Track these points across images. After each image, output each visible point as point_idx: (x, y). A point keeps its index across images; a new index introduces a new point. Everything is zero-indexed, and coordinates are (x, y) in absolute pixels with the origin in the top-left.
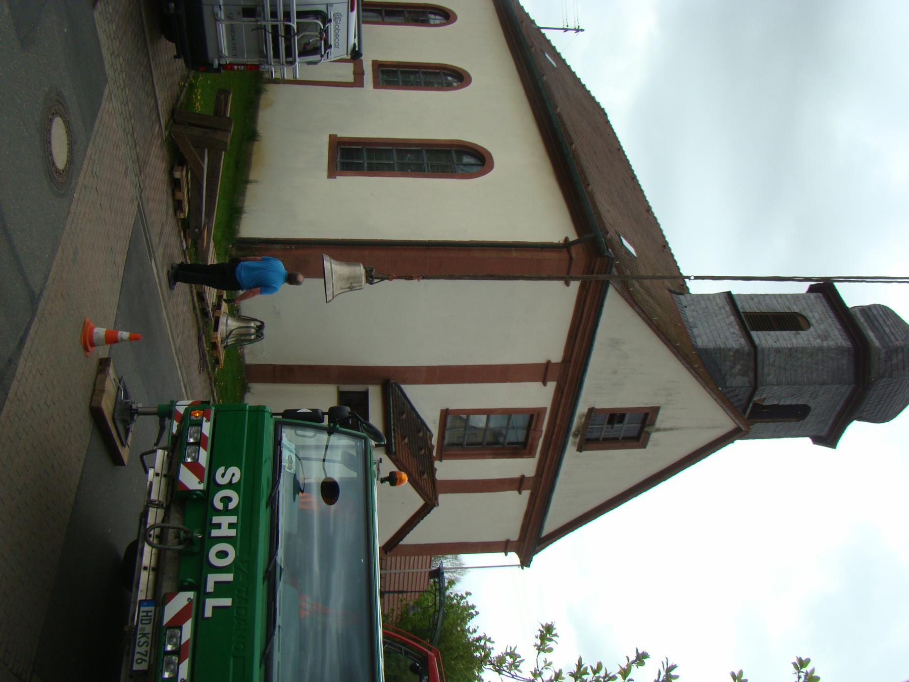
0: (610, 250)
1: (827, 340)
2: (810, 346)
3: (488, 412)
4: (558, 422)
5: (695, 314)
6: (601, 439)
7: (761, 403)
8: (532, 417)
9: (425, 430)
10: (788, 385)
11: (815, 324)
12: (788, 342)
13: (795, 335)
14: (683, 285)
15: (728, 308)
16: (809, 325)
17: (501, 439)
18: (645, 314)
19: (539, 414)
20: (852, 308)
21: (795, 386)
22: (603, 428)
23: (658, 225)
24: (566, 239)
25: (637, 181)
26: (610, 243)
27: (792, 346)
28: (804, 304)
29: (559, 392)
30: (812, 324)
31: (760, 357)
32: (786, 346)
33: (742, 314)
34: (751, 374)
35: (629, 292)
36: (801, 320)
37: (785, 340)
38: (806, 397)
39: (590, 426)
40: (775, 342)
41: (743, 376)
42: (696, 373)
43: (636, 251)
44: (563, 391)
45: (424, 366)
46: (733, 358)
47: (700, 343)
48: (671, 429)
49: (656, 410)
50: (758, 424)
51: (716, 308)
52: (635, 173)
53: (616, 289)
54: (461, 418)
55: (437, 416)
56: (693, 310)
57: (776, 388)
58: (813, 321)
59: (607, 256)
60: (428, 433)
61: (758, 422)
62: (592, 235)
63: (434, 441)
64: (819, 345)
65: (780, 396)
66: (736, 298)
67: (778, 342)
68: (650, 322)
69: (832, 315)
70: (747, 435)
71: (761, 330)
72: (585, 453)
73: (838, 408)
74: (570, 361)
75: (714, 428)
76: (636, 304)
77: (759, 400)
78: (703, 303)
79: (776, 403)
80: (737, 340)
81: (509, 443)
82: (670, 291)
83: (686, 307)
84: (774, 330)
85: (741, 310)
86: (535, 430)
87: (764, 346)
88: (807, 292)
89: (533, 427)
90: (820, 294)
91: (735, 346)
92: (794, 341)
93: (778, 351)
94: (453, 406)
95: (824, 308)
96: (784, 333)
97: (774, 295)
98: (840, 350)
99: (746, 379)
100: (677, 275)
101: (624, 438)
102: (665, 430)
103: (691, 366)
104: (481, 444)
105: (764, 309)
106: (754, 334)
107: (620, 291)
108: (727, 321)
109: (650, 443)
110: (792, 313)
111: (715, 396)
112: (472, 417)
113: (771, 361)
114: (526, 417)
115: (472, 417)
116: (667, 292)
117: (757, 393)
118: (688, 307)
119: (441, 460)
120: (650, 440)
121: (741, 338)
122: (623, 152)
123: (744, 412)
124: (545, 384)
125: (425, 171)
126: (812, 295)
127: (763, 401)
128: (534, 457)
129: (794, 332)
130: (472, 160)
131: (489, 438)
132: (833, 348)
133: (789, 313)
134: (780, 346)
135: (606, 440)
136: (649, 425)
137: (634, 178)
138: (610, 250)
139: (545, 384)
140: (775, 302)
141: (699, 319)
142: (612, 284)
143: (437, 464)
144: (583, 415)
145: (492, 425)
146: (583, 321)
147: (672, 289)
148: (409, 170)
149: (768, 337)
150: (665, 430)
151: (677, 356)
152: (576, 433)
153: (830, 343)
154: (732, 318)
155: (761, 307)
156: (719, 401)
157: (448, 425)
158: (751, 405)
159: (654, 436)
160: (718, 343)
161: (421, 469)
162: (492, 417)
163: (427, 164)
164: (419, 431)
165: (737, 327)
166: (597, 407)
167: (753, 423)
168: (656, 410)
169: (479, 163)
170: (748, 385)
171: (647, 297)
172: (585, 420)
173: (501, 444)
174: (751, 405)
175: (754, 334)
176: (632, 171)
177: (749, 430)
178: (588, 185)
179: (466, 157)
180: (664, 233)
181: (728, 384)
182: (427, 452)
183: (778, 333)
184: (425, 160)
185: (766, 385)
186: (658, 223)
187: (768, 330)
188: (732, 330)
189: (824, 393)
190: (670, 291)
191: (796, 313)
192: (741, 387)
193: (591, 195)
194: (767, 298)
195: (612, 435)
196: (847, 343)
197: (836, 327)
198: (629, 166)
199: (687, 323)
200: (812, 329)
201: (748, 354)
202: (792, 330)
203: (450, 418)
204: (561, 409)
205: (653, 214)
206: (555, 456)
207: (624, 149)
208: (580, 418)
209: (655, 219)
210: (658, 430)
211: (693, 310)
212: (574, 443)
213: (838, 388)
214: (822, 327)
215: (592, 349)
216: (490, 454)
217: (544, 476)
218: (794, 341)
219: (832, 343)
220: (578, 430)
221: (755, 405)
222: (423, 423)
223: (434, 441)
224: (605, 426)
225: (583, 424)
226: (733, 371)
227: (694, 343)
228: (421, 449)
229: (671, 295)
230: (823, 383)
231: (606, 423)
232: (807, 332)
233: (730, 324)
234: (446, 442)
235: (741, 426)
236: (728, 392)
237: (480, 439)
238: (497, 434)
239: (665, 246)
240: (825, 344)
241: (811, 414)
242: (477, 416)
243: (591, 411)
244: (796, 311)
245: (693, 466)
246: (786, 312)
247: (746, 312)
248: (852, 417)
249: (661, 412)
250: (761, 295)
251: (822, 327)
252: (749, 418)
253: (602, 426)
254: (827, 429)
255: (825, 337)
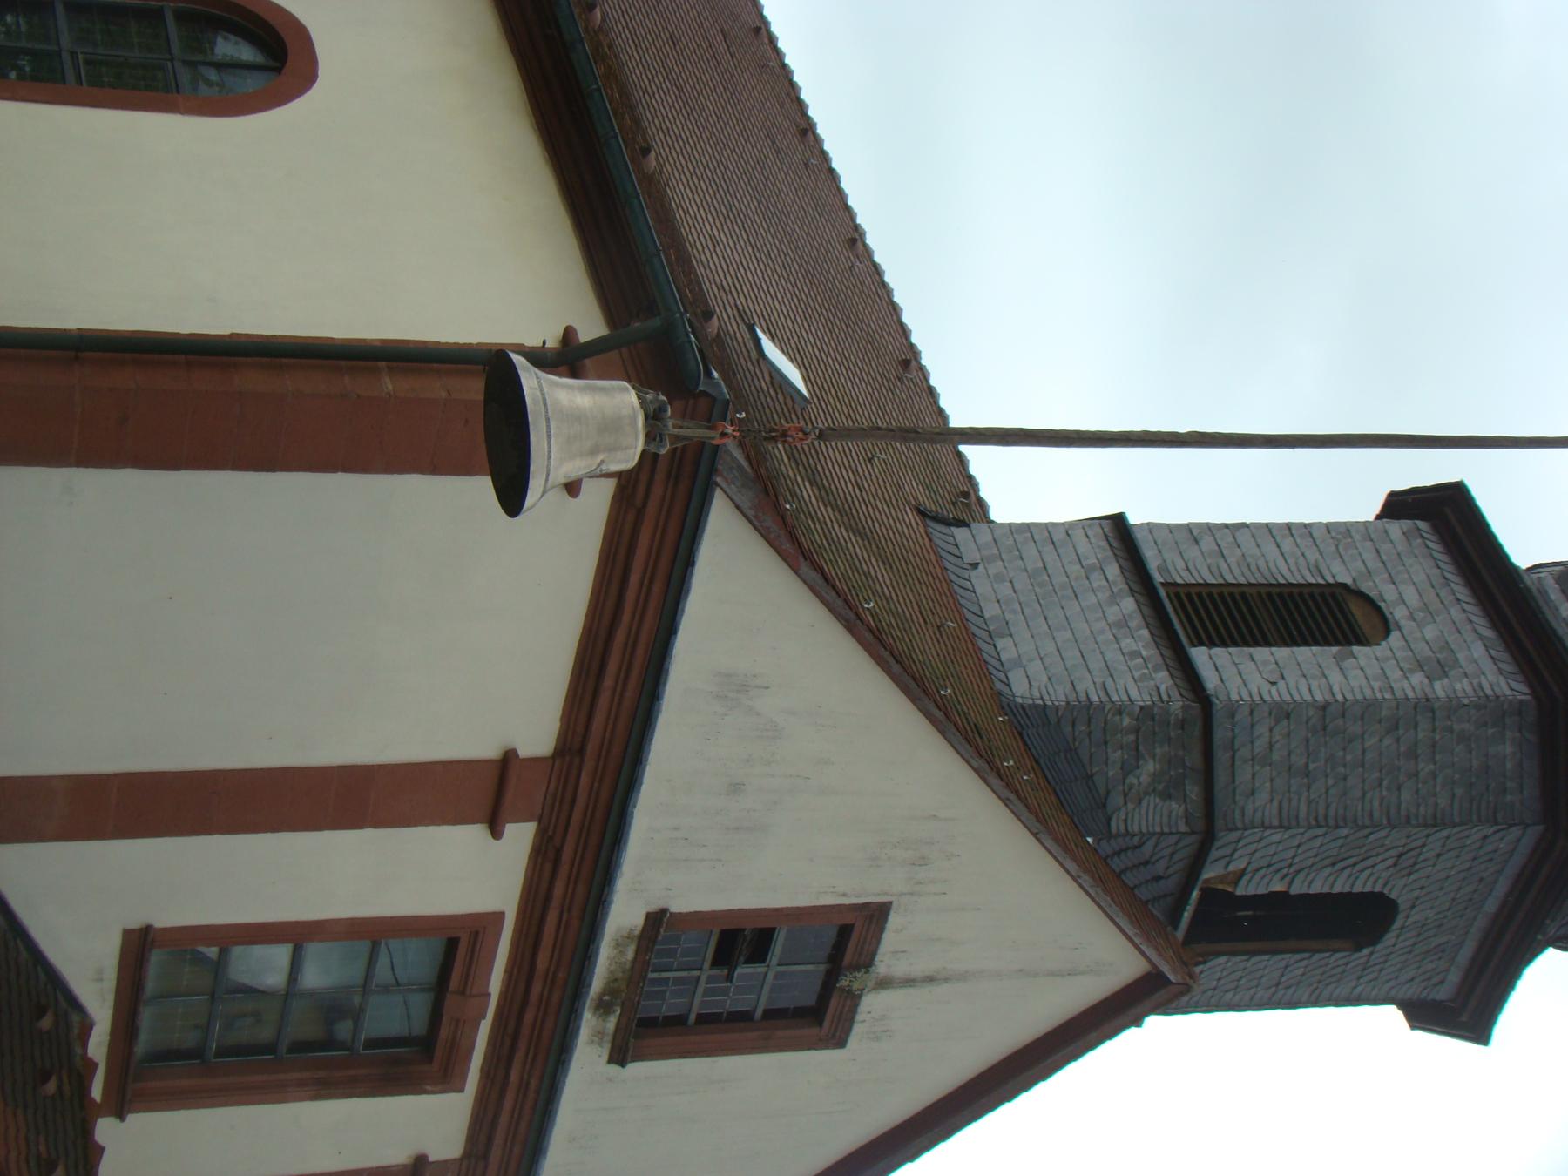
0: (716, 374)
1: (1445, 674)
2: (1388, 696)
3: (297, 935)
4: (542, 962)
5: (1005, 590)
6: (692, 1018)
7: (1229, 889)
8: (452, 945)
9: (63, 1004)
10: (1319, 826)
11: (1407, 625)
12: (1314, 684)
13: (1338, 659)
14: (966, 495)
15: (1113, 570)
16: (1385, 626)
17: (343, 1029)
18: (834, 587)
19: (475, 936)
20: (1529, 569)
21: (1345, 832)
22: (698, 978)
23: (882, 291)
24: (569, 333)
25: (818, 141)
26: (717, 351)
27: (1328, 697)
28: (1369, 556)
29: (544, 856)
30: (1397, 623)
31: (1220, 735)
32: (1307, 697)
33: (1162, 592)
34: (1194, 791)
35: (782, 516)
36: (1357, 610)
37: (1304, 676)
38: (1380, 867)
39: (651, 975)
40: (1273, 683)
41: (1166, 796)
42: (1009, 786)
43: (806, 378)
44: (559, 852)
45: (62, 777)
46: (1132, 737)
47: (1021, 688)
48: (930, 979)
49: (877, 914)
50: (1223, 959)
51: (1075, 569)
52: (812, 113)
53: (738, 508)
54: (200, 959)
55: (108, 952)
56: (999, 578)
57: (1276, 838)
58: (1399, 614)
59: (705, 393)
60: (75, 1018)
61: (1219, 954)
62: (656, 322)
63: (98, 1046)
64: (1420, 694)
65: (1290, 866)
66: (1139, 536)
67: (1281, 684)
68: (852, 616)
69: (1463, 592)
70: (1185, 998)
71: (1224, 645)
72: (636, 1069)
73: (1491, 906)
74: (581, 751)
75: (1072, 973)
76: (806, 555)
77: (1221, 879)
78: (1030, 552)
79: (1278, 887)
80: (1144, 677)
81: (372, 1043)
82: (922, 514)
83: (975, 566)
84: (1267, 643)
85: (1158, 578)
86: (462, 992)
87: (1235, 697)
88: (1378, 517)
89: (455, 981)
90: (1421, 524)
91: (1140, 697)
92: (1335, 678)
93: (1283, 712)
94: (169, 916)
95: (1437, 571)
96: (1304, 653)
97: (1268, 527)
98: (1492, 711)
99: (1176, 807)
100: (929, 423)
101: (770, 1014)
102: (908, 982)
103: (990, 764)
104: (270, 1048)
105: (1235, 574)
106: (1200, 656)
107: (750, 513)
108: (1113, 613)
109: (858, 1029)
110: (1328, 585)
111: (1072, 867)
112: (237, 951)
113: (1260, 745)
114: (437, 945)
115: (237, 951)
116: (911, 516)
117: (1214, 854)
118: (981, 567)
119: (121, 1116)
120: (859, 1017)
121: (1156, 669)
122: (772, 40)
123: (1174, 919)
124: (496, 833)
125: (64, 81)
126: (1396, 528)
127: (1236, 883)
128: (461, 1090)
129: (1335, 649)
130: (246, 53)
131: (302, 1026)
132: (1466, 701)
133: (1318, 585)
134: (1287, 697)
135: (707, 1020)
136: (856, 967)
137: (806, 130)
138: (716, 374)
139: (496, 833)
140: (1270, 549)
141: (1017, 606)
142: (722, 489)
143: (106, 1130)
144: (629, 937)
145: (314, 977)
146: (626, 618)
147: (929, 506)
148: (13, 75)
149: (1248, 667)
150: (908, 982)
151: (943, 733)
152: (606, 998)
153: (1458, 686)
154: (1129, 604)
155: (1224, 567)
156: (1086, 880)
157: (150, 986)
158: (1195, 894)
159: (872, 1004)
160: (1080, 687)
161: (42, 1148)
162: (313, 950)
163: (73, 55)
164: (41, 1011)
165: (1145, 633)
166: (678, 906)
167: (1205, 958)
168: (877, 914)
169: (271, 63)
170: (1183, 828)
171: (839, 532)
172: (637, 952)
173: (342, 1046)
174: (1195, 894)
175: (1200, 656)
176: (801, 107)
177: (1190, 982)
178: (646, 151)
179: (226, 39)
180: (906, 319)
181: (1116, 825)
182: (66, 1088)
183: (1282, 653)
184: (66, 40)
185: (1246, 829)
186: (884, 285)
187: (1247, 644)
188: (1128, 644)
189: (1439, 855)
190: (922, 514)
191: (1344, 586)
192: (1162, 833)
193: (654, 186)
194: (1243, 537)
195: (733, 1001)
196: (1513, 684)
197: (1476, 632)
198: (793, 88)
199: (980, 621)
200: (1395, 637)
201: (1182, 724)
202: (1329, 644)
203: (156, 958)
204: (552, 917)
205: (868, 252)
206: (534, 1083)
207: (774, 29)
208: (619, 945)
209: (877, 270)
210: (885, 983)
211: (999, 578)
212: (599, 1034)
213: (1485, 837)
214: (1430, 632)
215: (659, 710)
216: (301, 1084)
217: (496, 1154)
218: (1335, 678)
219: (1463, 687)
220: (611, 990)
221: (1209, 894)
222: (55, 980)
223: (98, 1046)
224: (707, 972)
225: (628, 966)
226: (1132, 780)
227: (999, 686)
228: (45, 1078)
229: (925, 526)
230: (1437, 822)
231: (707, 965)
232: (1381, 650)
233: (1123, 623)
234: (141, 1047)
235: (1165, 969)
236: (1118, 853)
237: (266, 1034)
238: (333, 1007)
239: (909, 360)
240: (1440, 689)
241: (1398, 924)
242: (258, 951)
243: (657, 920)
244: (1340, 580)
245: (1006, 1109)
246: (1309, 585)
247: (1176, 585)
248: (1539, 937)
249: (894, 921)
250: (1226, 526)
251: (1430, 632)
252: (1190, 938)
253: (696, 973)
254: (1454, 977)
255: (1440, 667)
